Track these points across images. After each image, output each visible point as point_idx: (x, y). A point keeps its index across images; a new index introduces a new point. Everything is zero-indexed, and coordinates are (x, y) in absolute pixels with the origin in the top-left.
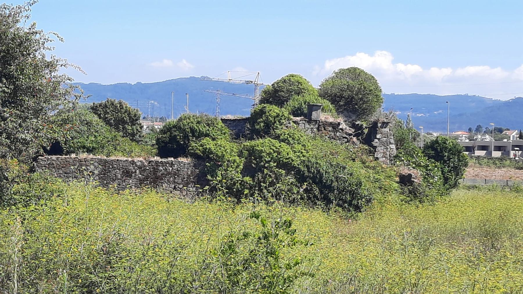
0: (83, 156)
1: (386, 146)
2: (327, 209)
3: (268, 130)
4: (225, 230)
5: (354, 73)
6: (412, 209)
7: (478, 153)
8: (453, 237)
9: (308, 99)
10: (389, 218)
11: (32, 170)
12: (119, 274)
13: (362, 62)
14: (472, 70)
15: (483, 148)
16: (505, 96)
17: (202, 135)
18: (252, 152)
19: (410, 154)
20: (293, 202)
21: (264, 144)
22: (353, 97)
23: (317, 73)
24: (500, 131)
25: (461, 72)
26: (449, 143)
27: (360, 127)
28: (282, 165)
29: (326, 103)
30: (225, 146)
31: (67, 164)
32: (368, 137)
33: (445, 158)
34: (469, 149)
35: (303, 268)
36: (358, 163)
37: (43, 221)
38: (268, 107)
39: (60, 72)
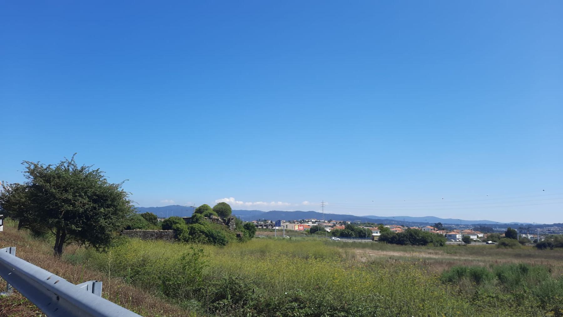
0: (138, 230)
1: (232, 225)
2: (214, 245)
3: (197, 221)
4: (181, 253)
5: (223, 204)
6: (240, 244)
7: (260, 227)
8: (252, 253)
9: (209, 211)
10: (234, 247)
11: (121, 235)
12: (148, 268)
13: (226, 201)
14: (258, 203)
15: (261, 226)
16: (267, 210)
17: (176, 223)
18: (192, 228)
19: (239, 228)
20: (204, 243)
21: (196, 226)
22: (223, 211)
23: (212, 204)
24: (266, 221)
25: (255, 204)
26: (251, 224)
27: (225, 220)
28: (201, 232)
29: (215, 213)
30: (183, 226)
31: (132, 232)
32: (227, 223)
33: (250, 229)
34: (257, 226)
35: (206, 264)
36: (224, 231)
37: (123, 251)
38: (197, 214)
39: (131, 204)
